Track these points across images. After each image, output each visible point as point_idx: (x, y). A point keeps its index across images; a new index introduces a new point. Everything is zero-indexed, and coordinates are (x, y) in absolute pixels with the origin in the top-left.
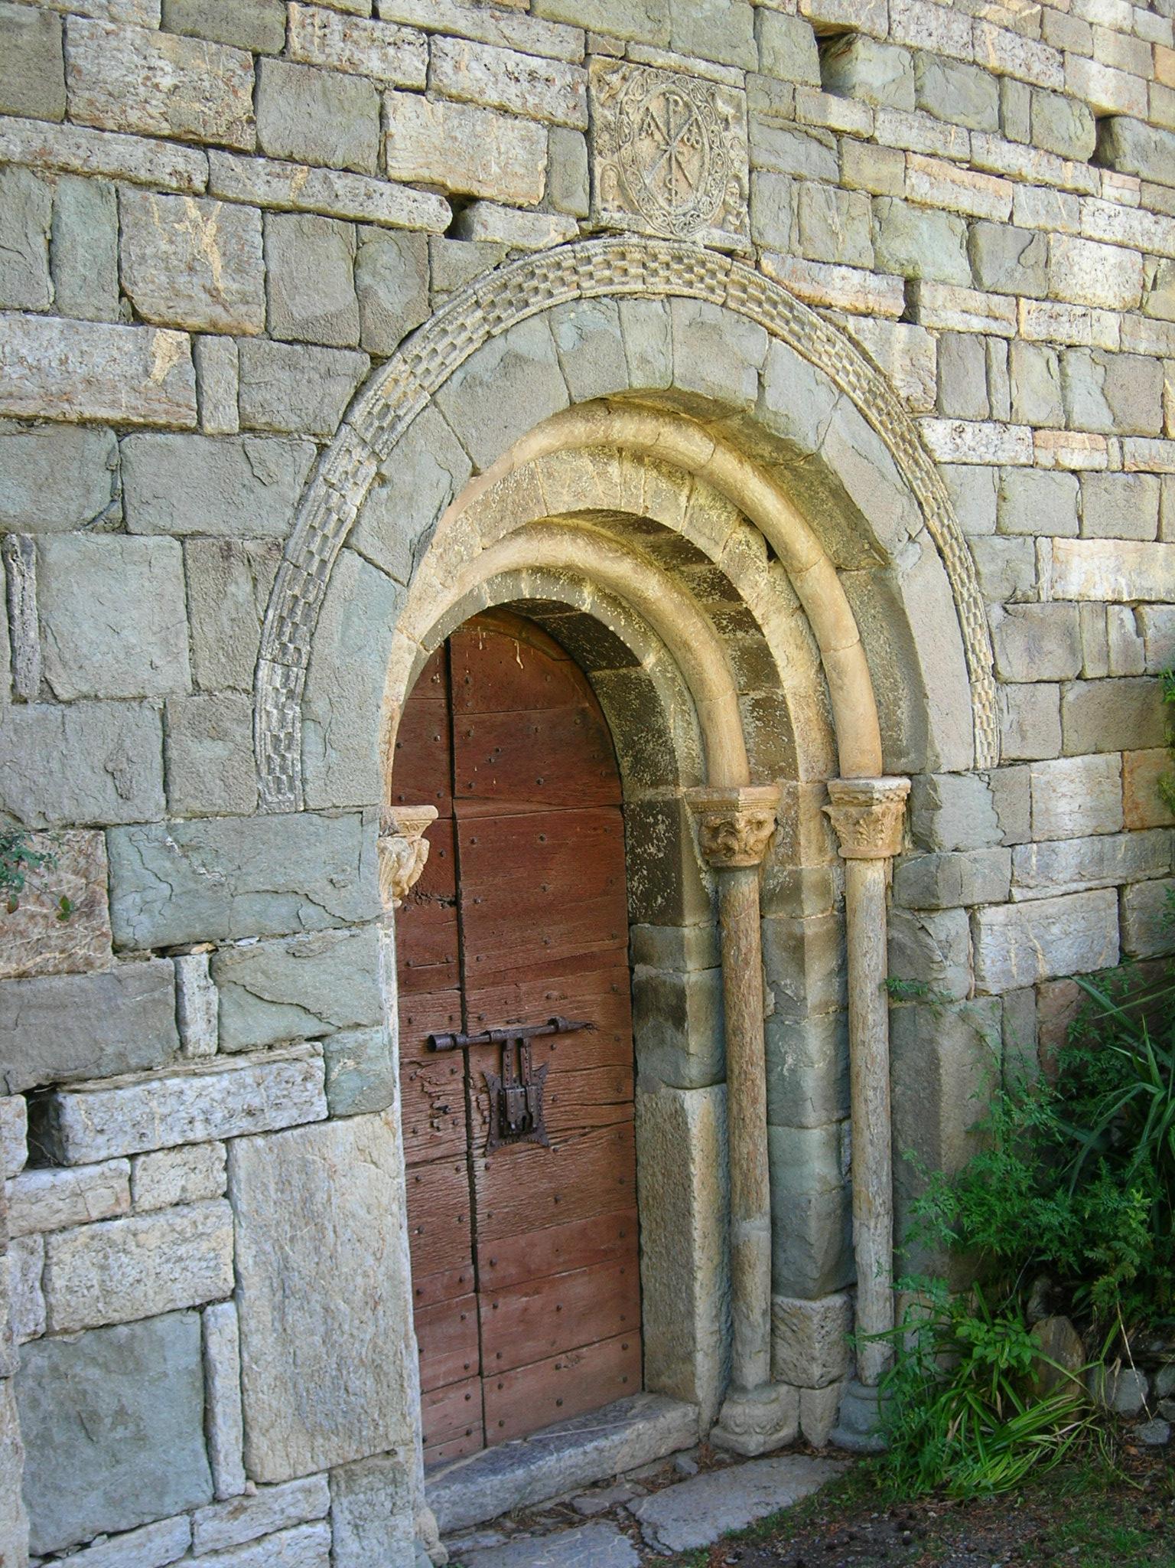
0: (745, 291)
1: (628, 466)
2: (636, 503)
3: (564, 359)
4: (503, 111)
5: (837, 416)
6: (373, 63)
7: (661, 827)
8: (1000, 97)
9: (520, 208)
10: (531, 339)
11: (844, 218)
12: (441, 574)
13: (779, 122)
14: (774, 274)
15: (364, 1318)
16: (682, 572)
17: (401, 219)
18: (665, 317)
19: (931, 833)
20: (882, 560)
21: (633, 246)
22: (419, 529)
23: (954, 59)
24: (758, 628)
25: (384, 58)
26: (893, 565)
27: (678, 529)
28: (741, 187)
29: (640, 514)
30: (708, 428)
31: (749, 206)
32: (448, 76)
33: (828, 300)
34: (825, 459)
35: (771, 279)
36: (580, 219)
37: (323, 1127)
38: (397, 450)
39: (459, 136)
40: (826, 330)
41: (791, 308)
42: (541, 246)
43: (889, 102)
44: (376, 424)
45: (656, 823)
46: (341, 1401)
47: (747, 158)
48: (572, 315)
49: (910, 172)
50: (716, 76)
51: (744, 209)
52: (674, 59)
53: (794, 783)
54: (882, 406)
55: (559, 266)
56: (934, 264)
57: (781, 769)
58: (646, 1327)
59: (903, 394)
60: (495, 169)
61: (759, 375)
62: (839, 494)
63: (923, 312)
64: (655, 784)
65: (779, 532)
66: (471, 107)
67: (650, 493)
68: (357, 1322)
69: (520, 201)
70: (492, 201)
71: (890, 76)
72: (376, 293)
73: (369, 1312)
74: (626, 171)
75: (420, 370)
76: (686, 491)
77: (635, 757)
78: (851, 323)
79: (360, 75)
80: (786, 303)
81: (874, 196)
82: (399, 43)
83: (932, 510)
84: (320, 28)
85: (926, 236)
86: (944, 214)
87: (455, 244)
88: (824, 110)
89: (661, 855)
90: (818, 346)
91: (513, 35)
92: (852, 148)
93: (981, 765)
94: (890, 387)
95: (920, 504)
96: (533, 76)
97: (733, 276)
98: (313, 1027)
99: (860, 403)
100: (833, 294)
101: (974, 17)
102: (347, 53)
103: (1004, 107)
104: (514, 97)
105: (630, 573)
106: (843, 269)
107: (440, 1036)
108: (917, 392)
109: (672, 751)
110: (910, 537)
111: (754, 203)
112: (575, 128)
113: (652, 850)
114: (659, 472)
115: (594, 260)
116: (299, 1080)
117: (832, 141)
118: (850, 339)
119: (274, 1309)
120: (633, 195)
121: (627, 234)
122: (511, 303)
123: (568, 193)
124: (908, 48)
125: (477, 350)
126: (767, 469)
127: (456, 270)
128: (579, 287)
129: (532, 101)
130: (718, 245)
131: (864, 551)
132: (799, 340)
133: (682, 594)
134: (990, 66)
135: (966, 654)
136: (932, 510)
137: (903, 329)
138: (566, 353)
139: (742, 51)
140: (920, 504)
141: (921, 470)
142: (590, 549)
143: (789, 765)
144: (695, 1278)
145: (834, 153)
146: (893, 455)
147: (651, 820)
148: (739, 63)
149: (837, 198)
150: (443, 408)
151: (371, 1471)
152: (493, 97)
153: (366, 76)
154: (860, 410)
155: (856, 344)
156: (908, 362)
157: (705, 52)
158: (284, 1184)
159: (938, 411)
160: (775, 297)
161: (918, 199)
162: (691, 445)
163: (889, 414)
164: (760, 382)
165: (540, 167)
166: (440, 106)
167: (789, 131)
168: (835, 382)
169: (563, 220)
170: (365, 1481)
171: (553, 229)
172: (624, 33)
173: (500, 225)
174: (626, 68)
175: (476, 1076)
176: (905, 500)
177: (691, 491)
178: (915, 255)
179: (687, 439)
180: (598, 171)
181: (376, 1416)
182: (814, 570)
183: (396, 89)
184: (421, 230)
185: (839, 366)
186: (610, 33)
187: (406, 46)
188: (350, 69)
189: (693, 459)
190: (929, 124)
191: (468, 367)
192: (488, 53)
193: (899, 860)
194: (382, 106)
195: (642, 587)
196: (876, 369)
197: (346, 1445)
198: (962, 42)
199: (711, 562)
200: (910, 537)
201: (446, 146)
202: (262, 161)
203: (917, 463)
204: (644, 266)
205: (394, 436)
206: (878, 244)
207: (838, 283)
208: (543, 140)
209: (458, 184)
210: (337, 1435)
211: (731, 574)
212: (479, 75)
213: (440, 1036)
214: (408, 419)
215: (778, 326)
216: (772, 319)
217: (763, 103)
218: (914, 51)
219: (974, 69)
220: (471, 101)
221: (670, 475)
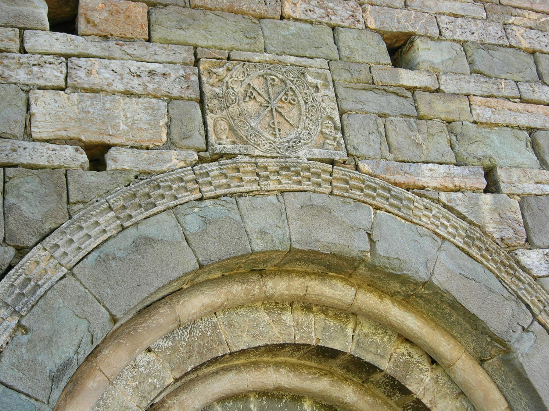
0: (347, 183)
1: (299, 315)
2: (309, 337)
3: (190, 238)
4: (129, 94)
5: (442, 256)
8: (536, 63)
9: (147, 149)
10: (163, 227)
11: (425, 135)
12: (137, 399)
13: (362, 85)
14: (371, 171)
16: (372, 382)
17: (42, 162)
18: (278, 204)
20: (506, 349)
21: (245, 163)
22: (58, 362)
23: (494, 45)
25: (30, 73)
26: (513, 349)
27: (348, 351)
28: (334, 123)
29: (314, 343)
30: (353, 280)
31: (343, 133)
32: (80, 76)
33: (420, 184)
34: (436, 283)
35: (370, 175)
36: (199, 151)
38: (36, 308)
39: (91, 111)
40: (420, 202)
41: (389, 191)
42: (165, 168)
43: (449, 69)
44: (17, 291)
47: (336, 106)
48: (196, 209)
49: (474, 107)
50: (305, 64)
51: (339, 135)
52: (268, 56)
54: (480, 244)
55: (181, 180)
56: (506, 157)
59: (496, 236)
60: (122, 127)
61: (369, 235)
62: (455, 305)
63: (502, 185)
65: (425, 342)
66: (102, 94)
67: (320, 330)
69: (145, 144)
70: (122, 146)
71: (447, 56)
72: (19, 208)
74: (234, 120)
75: (58, 253)
76: (351, 326)
78: (443, 197)
80: (384, 188)
81: (449, 123)
82: (42, 64)
83: (539, 308)
85: (497, 142)
86: (509, 129)
90: (416, 212)
92: (423, 98)
94: (485, 233)
95: (528, 306)
96: (151, 73)
97: (334, 175)
99: (461, 245)
100: (424, 180)
101: (505, 24)
103: (540, 68)
104: (137, 86)
105: (328, 387)
106: (430, 165)
108: (510, 234)
110: (523, 328)
111: (346, 131)
112: (190, 99)
114: (326, 315)
115: (211, 174)
117: (409, 94)
118: (445, 206)
120: (242, 133)
121: (239, 157)
122: (140, 206)
123: (186, 137)
124: (458, 42)
126: (383, 292)
127: (89, 188)
128: (200, 191)
129: (151, 87)
130: (319, 157)
131: (489, 344)
132: (399, 209)
133: (374, 396)
134: (523, 47)
136: (539, 308)
137: (488, 198)
138: (192, 234)
139: (324, 49)
140: (528, 306)
141: (524, 283)
142: (291, 375)
145: (411, 100)
146: (497, 276)
148: (322, 55)
149: (417, 125)
150: (79, 277)
152: (119, 86)
153: (15, 84)
154: (462, 250)
155: (451, 209)
156: (497, 216)
157: (294, 51)
159: (529, 243)
160: (373, 185)
161: (484, 121)
162: (338, 291)
163: (488, 250)
164: (371, 239)
165: (162, 123)
166: (75, 96)
167: (370, 90)
168: (436, 234)
169: (184, 153)
171: (174, 159)
172: (226, 45)
173: (128, 159)
174: (229, 64)
176: (513, 304)
177: (356, 325)
178: (489, 153)
179: (331, 287)
180: (210, 122)
182: (459, 364)
183: (38, 89)
184: (60, 167)
185: (437, 222)
186: (215, 47)
187: (48, 65)
189: (341, 301)
190: (482, 79)
191: (102, 248)
192: (114, 64)
194: (28, 100)
195: (341, 395)
196: (470, 223)
198: (498, 36)
199: (382, 371)
200: (523, 328)
201: (80, 117)
203: (519, 280)
204: (258, 175)
205: (33, 300)
206: (457, 148)
207: (427, 173)
209: (92, 136)
211: (398, 375)
212: (107, 75)
214: (46, 287)
215: (379, 201)
216: (374, 198)
217: (346, 76)
218: (463, 43)
219: (511, 50)
220: (102, 90)
221: (336, 316)
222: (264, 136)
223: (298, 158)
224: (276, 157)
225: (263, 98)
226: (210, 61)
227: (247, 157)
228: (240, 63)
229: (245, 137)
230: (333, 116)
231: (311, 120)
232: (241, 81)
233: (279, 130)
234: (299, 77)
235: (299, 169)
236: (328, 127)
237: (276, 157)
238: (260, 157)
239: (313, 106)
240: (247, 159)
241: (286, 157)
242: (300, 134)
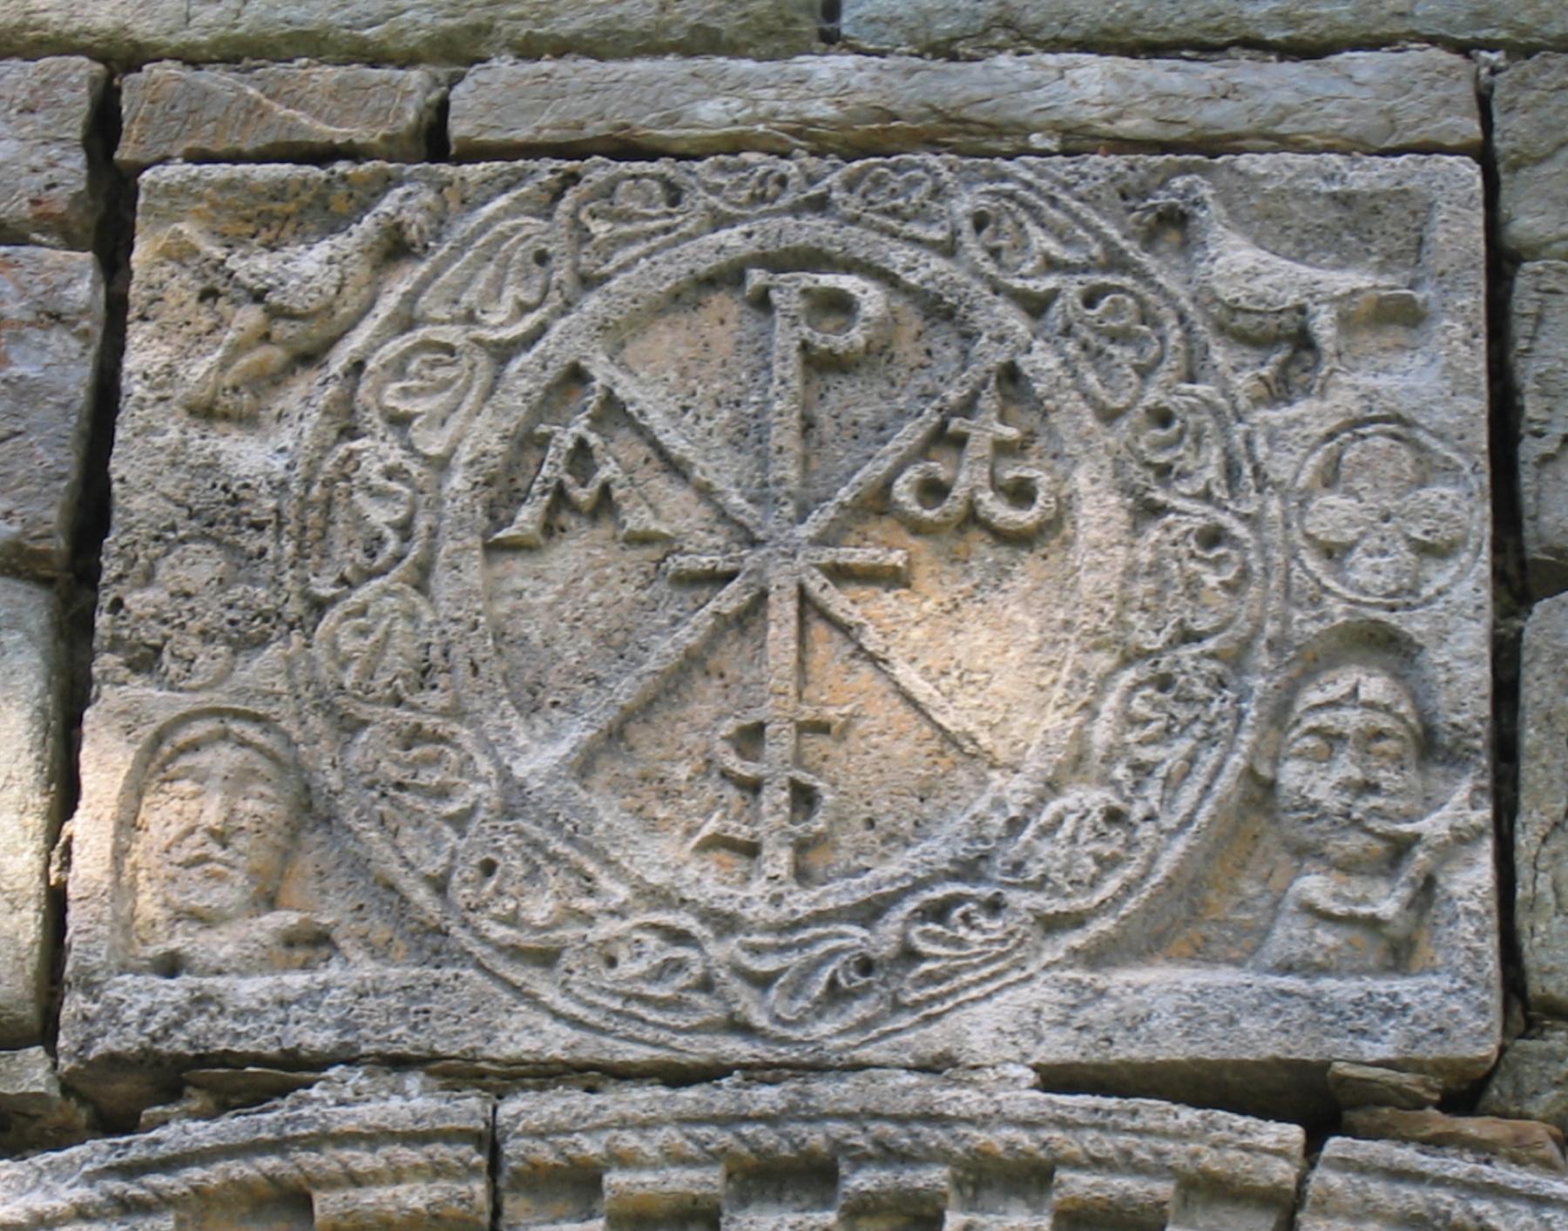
47: (1478, 520)
51: (1460, 804)
52: (828, 81)
130: (1174, 1049)
222: (620, 874)
223: (935, 1066)
224: (710, 1073)
225: (705, 492)
226: (229, 185)
227: (413, 1082)
228: (520, 178)
229: (420, 893)
230: (1415, 625)
231: (1164, 683)
232: (503, 353)
233: (804, 798)
234: (1116, 261)
235: (936, 1176)
236: (1332, 739)
237: (710, 1073)
238: (546, 1074)
239: (1213, 537)
240: (414, 1100)
241: (819, 1068)
242: (1015, 826)
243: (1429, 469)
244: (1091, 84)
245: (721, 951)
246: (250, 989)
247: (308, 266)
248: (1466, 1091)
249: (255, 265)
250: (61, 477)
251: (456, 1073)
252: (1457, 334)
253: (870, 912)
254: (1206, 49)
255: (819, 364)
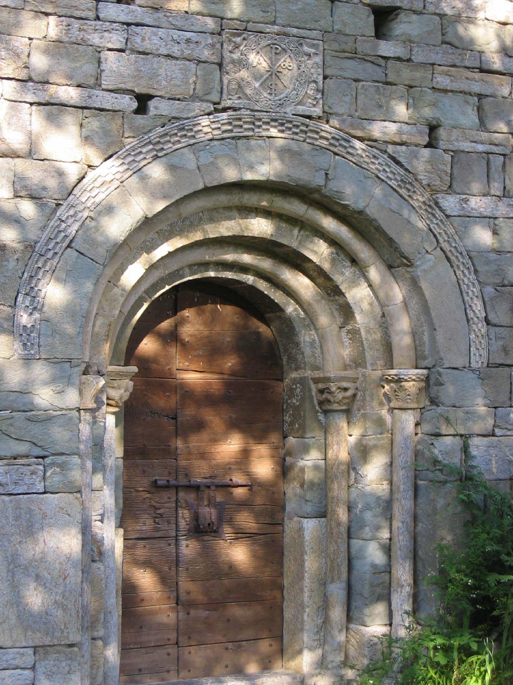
6: (95, 39)
7: (299, 390)
9: (179, 100)
15: (58, 583)
19: (437, 398)
24: (343, 294)
37: (41, 496)
42: (190, 116)
45: (296, 388)
46: (43, 617)
53: (365, 370)
57: (360, 363)
58: (284, 636)
64: (296, 369)
68: (54, 584)
73: (61, 580)
77: (288, 356)
79: (88, 45)
84: (66, 26)
87: (139, 116)
88: (376, 47)
89: (298, 403)
91: (177, 23)
93: (474, 365)
98: (38, 451)
102: (81, 36)
104: (176, 51)
107: (159, 480)
109: (303, 353)
113: (295, 401)
116: (29, 474)
119: (8, 571)
125: (149, 163)
130: (301, 113)
135: (465, 311)
137: (426, 152)
143: (363, 362)
144: (305, 611)
147: (294, 387)
151: (58, 652)
152: (164, 51)
153: (91, 45)
157: (297, 24)
158: (17, 518)
170: (55, 656)
175: (182, 501)
181: (63, 627)
188: (83, 43)
192: (161, 32)
193: (423, 410)
196: (406, 170)
197: (45, 637)
202: (31, 84)
208: (194, 70)
210: (40, 632)
213: (159, 480)
240: (248, 112)
243: (319, 68)
244: (295, 31)
245: (270, 102)
246: (236, 102)
247: (238, 40)
248: (320, 118)
249: (234, 39)
250: (355, 272)
251: (252, 110)
252: (321, 57)
253: (280, 100)
254: (303, 29)
255: (276, 53)
